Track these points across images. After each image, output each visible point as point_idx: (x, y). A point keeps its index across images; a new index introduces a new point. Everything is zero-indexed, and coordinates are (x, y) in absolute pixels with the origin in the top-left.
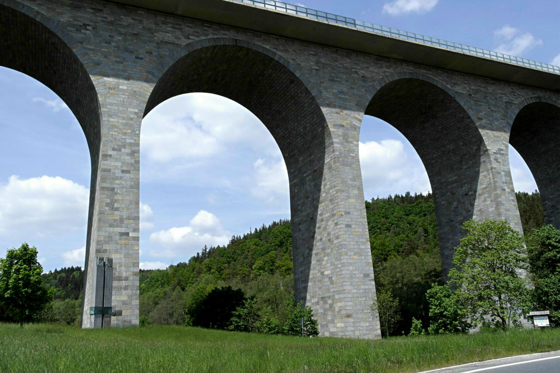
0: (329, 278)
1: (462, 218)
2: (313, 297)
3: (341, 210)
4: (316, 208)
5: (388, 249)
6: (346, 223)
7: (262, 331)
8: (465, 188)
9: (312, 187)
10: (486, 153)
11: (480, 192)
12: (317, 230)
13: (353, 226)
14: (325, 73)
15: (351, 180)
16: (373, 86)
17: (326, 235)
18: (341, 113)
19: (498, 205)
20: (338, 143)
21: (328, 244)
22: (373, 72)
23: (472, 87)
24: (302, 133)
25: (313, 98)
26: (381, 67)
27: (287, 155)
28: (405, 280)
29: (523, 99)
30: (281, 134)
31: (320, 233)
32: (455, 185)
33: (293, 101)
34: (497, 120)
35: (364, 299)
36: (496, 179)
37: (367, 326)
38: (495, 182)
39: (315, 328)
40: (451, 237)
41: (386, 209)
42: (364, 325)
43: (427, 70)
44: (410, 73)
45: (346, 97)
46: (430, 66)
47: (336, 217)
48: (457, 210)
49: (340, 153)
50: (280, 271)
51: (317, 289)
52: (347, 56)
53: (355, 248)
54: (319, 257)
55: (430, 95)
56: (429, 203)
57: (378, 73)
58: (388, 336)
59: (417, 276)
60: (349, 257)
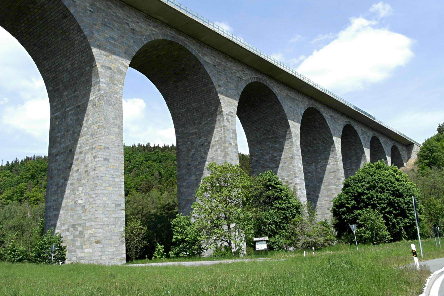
0: (82, 207)
1: (197, 163)
2: (64, 224)
3: (100, 144)
4: (76, 141)
5: (129, 186)
6: (104, 157)
7: (6, 258)
8: (202, 139)
9: (74, 121)
10: (221, 113)
11: (213, 144)
12: (74, 162)
13: (110, 160)
14: (99, 17)
15: (113, 118)
16: (141, 39)
17: (83, 167)
18: (110, 57)
19: (226, 154)
20: (105, 84)
21: (85, 175)
22: (142, 27)
23: (217, 60)
24: (69, 69)
25: (85, 37)
26: (149, 25)
27: (51, 88)
28: (144, 212)
29: (249, 77)
30: (47, 67)
31: (78, 165)
32: (194, 136)
33: (64, 37)
34: (231, 89)
35: (114, 227)
36: (226, 135)
37: (113, 251)
38: (225, 137)
39: (63, 254)
40: (187, 178)
41: (130, 154)
42: (112, 250)
43: (186, 38)
44: (172, 36)
45: (116, 43)
46: (189, 35)
47: (95, 151)
48: (194, 156)
49: (106, 93)
50: (29, 201)
51: (69, 217)
52: (121, 7)
53: (110, 180)
54: (73, 187)
55: (185, 59)
56: (164, 153)
57: (146, 30)
58: (134, 260)
59: (154, 208)
60: (104, 188)
